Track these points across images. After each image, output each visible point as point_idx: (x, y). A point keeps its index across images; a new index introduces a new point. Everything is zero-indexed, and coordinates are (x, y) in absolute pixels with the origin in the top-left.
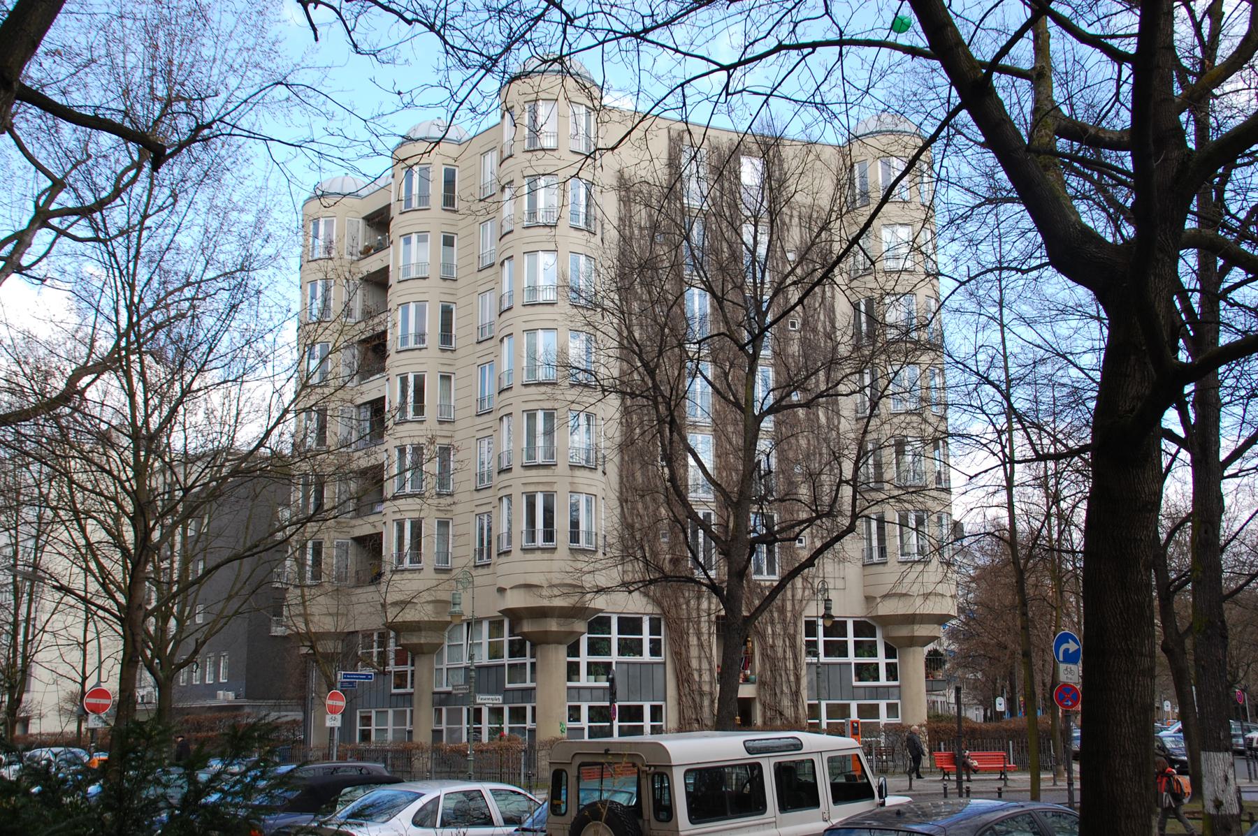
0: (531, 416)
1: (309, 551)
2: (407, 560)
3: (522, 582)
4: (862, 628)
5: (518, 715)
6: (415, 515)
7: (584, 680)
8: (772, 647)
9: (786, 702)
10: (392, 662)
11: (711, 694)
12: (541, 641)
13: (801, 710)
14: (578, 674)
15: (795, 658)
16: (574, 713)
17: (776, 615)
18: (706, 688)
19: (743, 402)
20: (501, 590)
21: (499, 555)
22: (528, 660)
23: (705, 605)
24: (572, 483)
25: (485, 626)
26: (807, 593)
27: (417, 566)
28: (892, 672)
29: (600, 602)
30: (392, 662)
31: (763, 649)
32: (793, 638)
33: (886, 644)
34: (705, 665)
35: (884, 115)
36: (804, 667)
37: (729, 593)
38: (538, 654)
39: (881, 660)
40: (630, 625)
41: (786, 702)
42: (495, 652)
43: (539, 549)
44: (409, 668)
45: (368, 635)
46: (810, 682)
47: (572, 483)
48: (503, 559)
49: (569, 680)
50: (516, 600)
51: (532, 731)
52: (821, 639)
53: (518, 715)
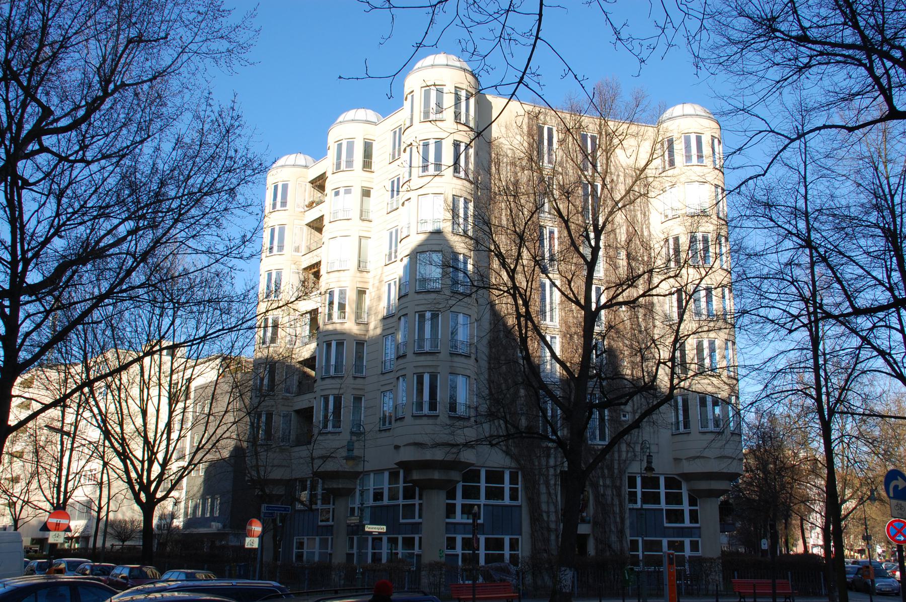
0: (422, 316)
1: (263, 418)
2: (330, 425)
3: (412, 441)
4: (672, 482)
5: (408, 543)
6: (336, 392)
7: (459, 518)
8: (603, 495)
9: (614, 538)
10: (319, 502)
11: (556, 530)
12: (427, 486)
13: (625, 545)
14: (455, 513)
15: (621, 505)
16: (451, 543)
17: (606, 471)
18: (553, 526)
19: (582, 302)
20: (397, 447)
21: (396, 420)
22: (417, 502)
23: (552, 462)
24: (451, 367)
25: (386, 474)
26: (629, 455)
27: (337, 430)
28: (694, 517)
29: (468, 456)
30: (319, 502)
31: (596, 497)
32: (619, 489)
33: (689, 495)
34: (552, 509)
36: (628, 511)
37: (573, 447)
38: (424, 497)
39: (686, 507)
40: (495, 476)
41: (614, 538)
42: (393, 496)
43: (425, 416)
44: (331, 507)
45: (303, 481)
46: (631, 523)
47: (451, 367)
48: (399, 423)
49: (448, 517)
50: (408, 455)
51: (419, 556)
52: (639, 490)
53: (408, 543)
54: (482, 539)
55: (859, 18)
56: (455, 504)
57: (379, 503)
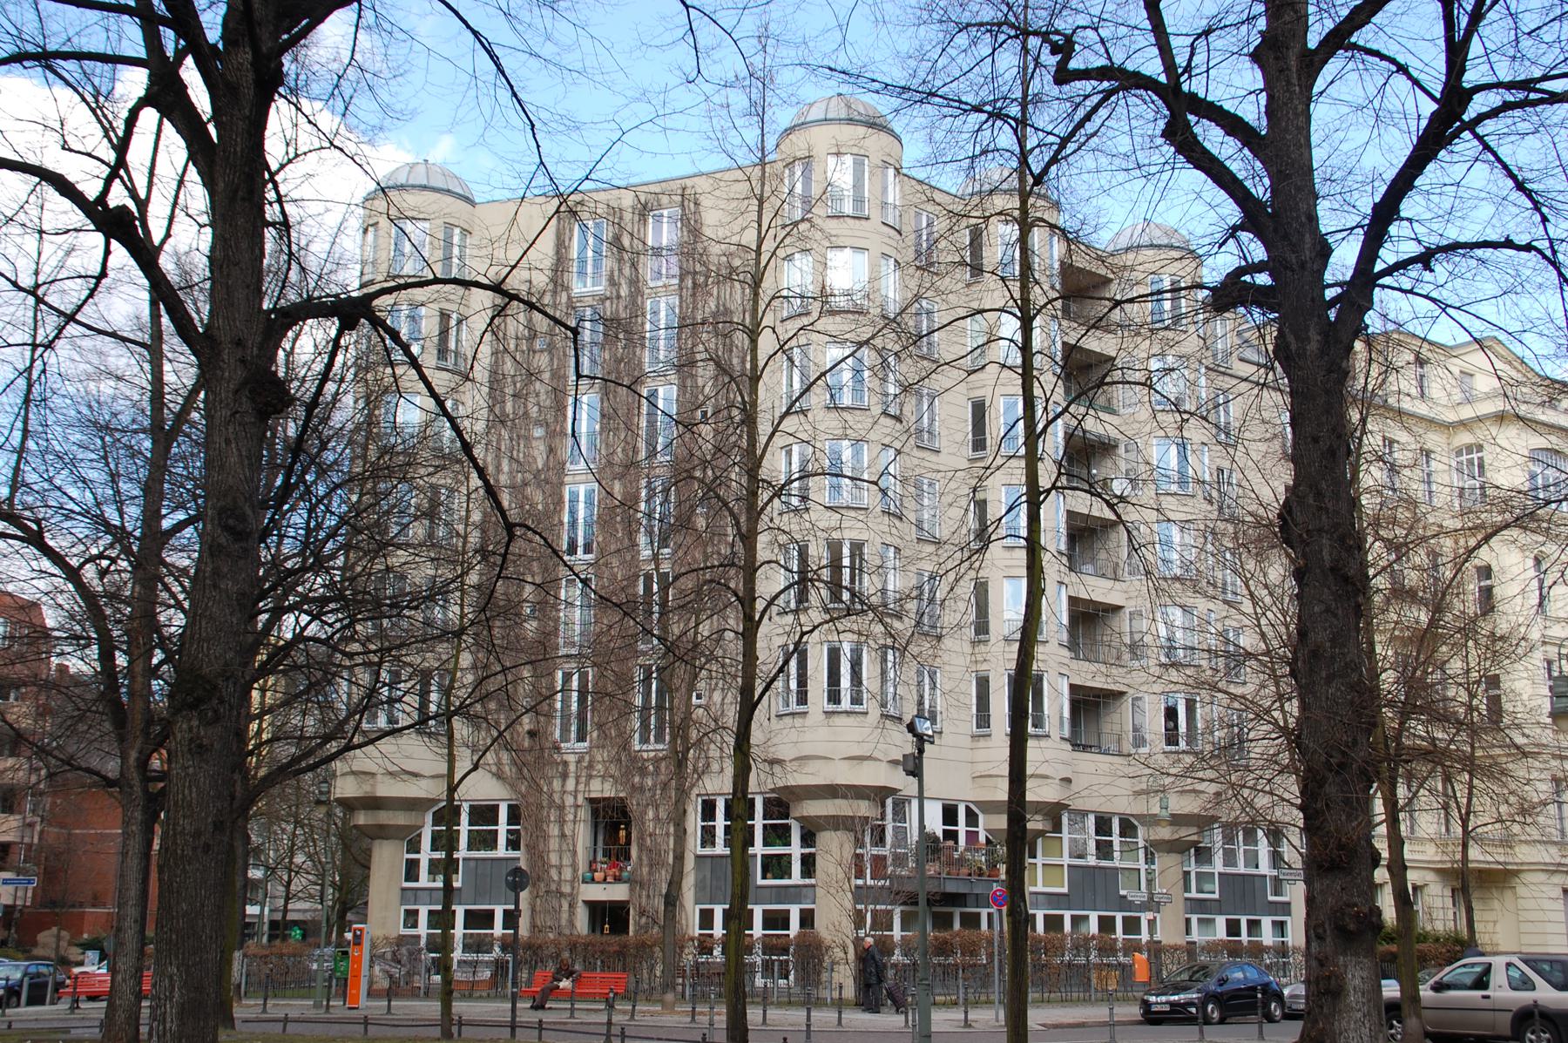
16: (411, 917)
28: (808, 864)
35: (879, 563)
39: (796, 850)
40: (484, 814)
43: (846, 712)
54: (460, 911)
55: (1292, 723)
56: (418, 861)
57: (708, 851)
